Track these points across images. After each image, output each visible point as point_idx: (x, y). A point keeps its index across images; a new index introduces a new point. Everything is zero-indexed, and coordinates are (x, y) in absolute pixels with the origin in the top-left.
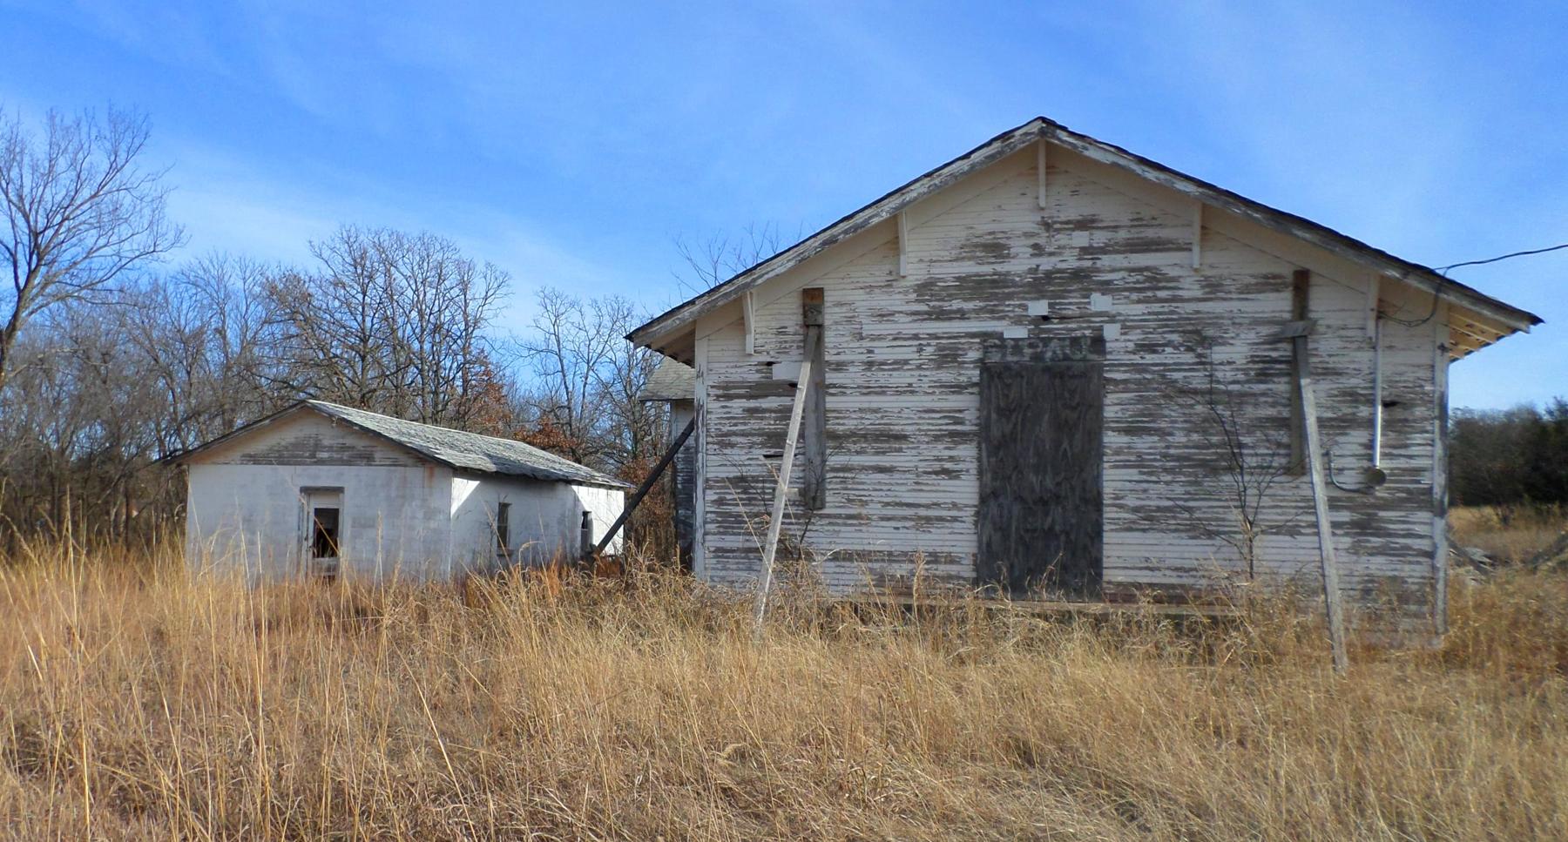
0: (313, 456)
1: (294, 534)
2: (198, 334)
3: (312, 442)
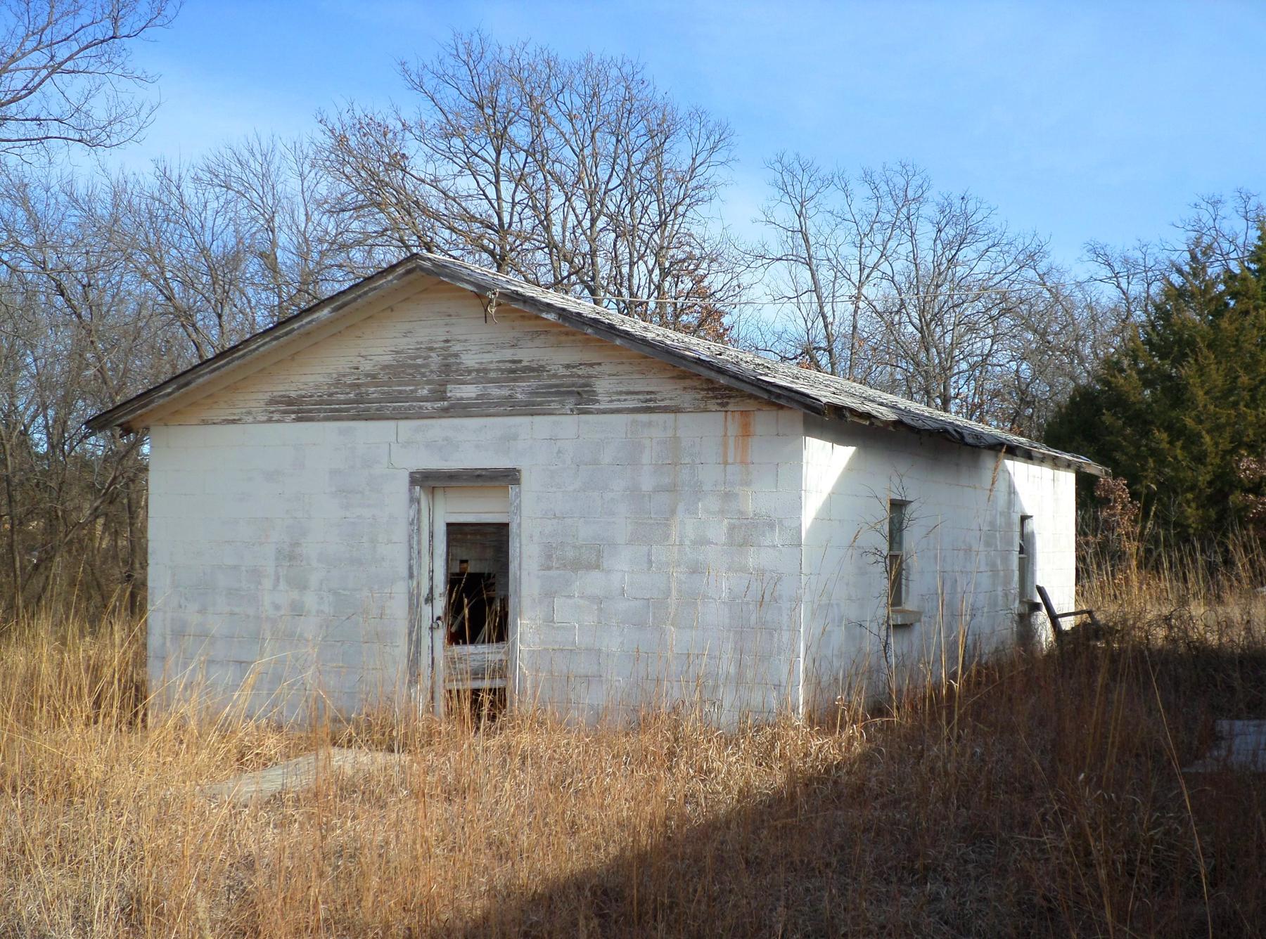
0: (439, 394)
1: (400, 590)
2: (234, 260)
3: (435, 359)
